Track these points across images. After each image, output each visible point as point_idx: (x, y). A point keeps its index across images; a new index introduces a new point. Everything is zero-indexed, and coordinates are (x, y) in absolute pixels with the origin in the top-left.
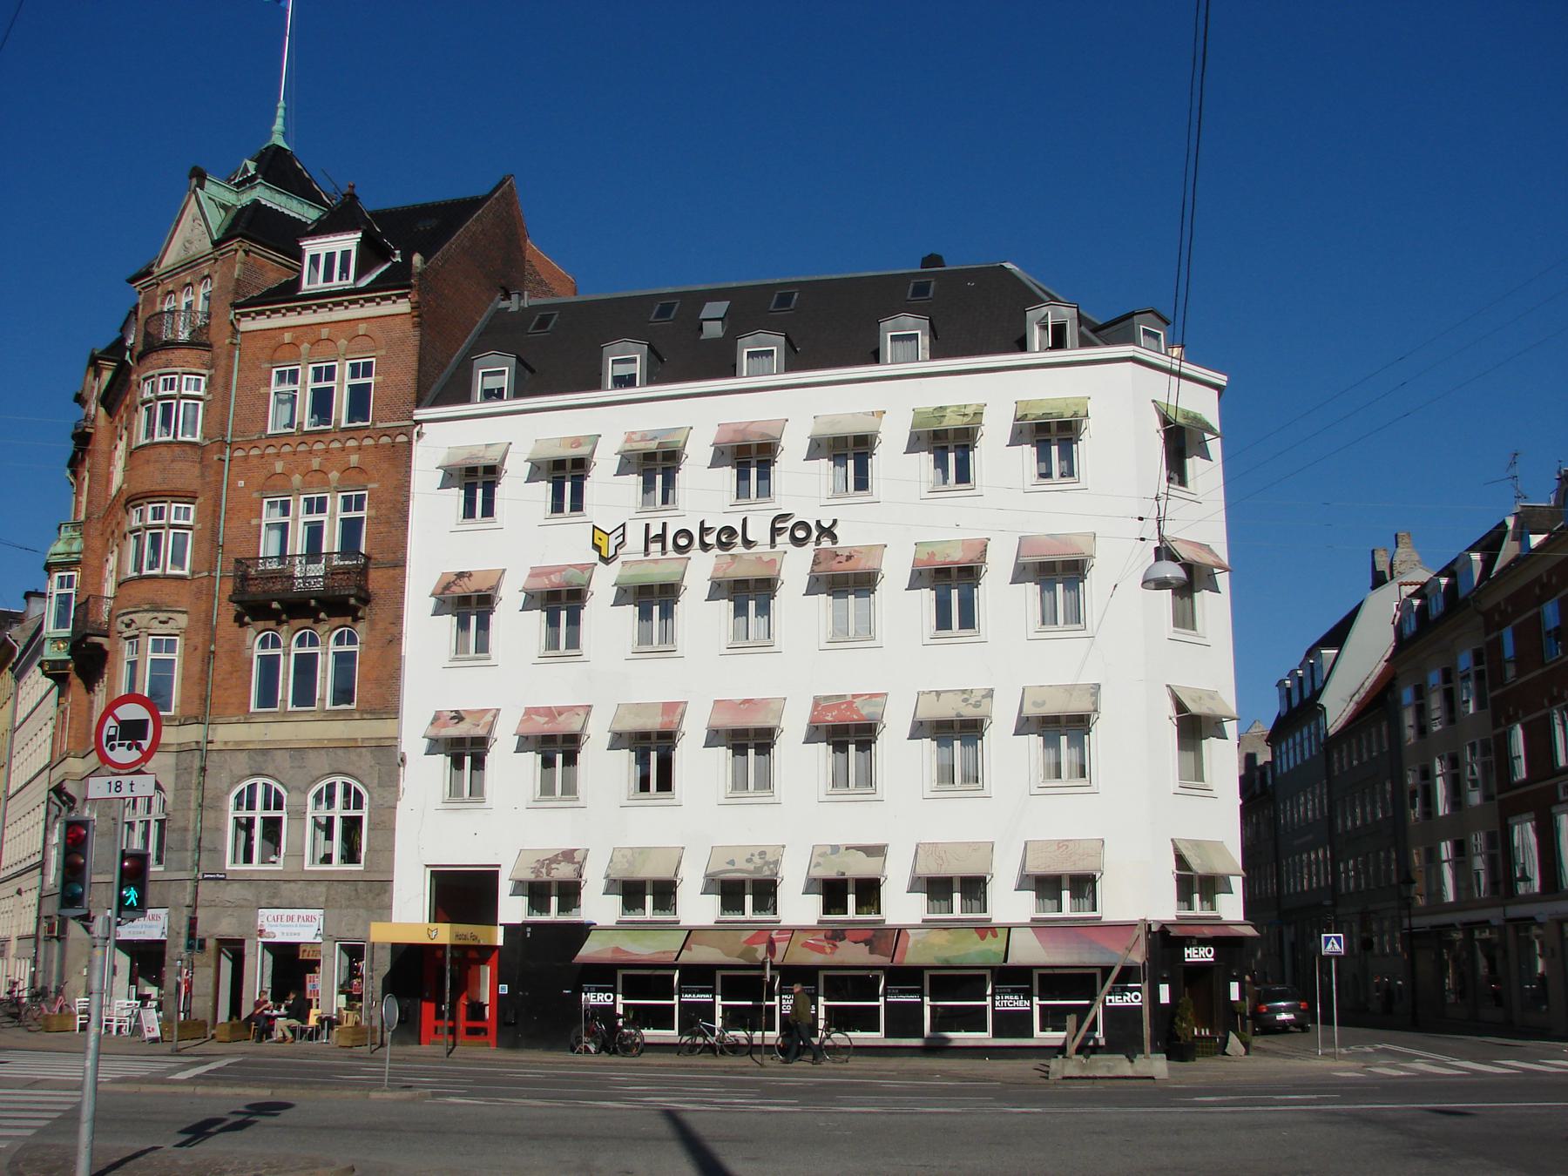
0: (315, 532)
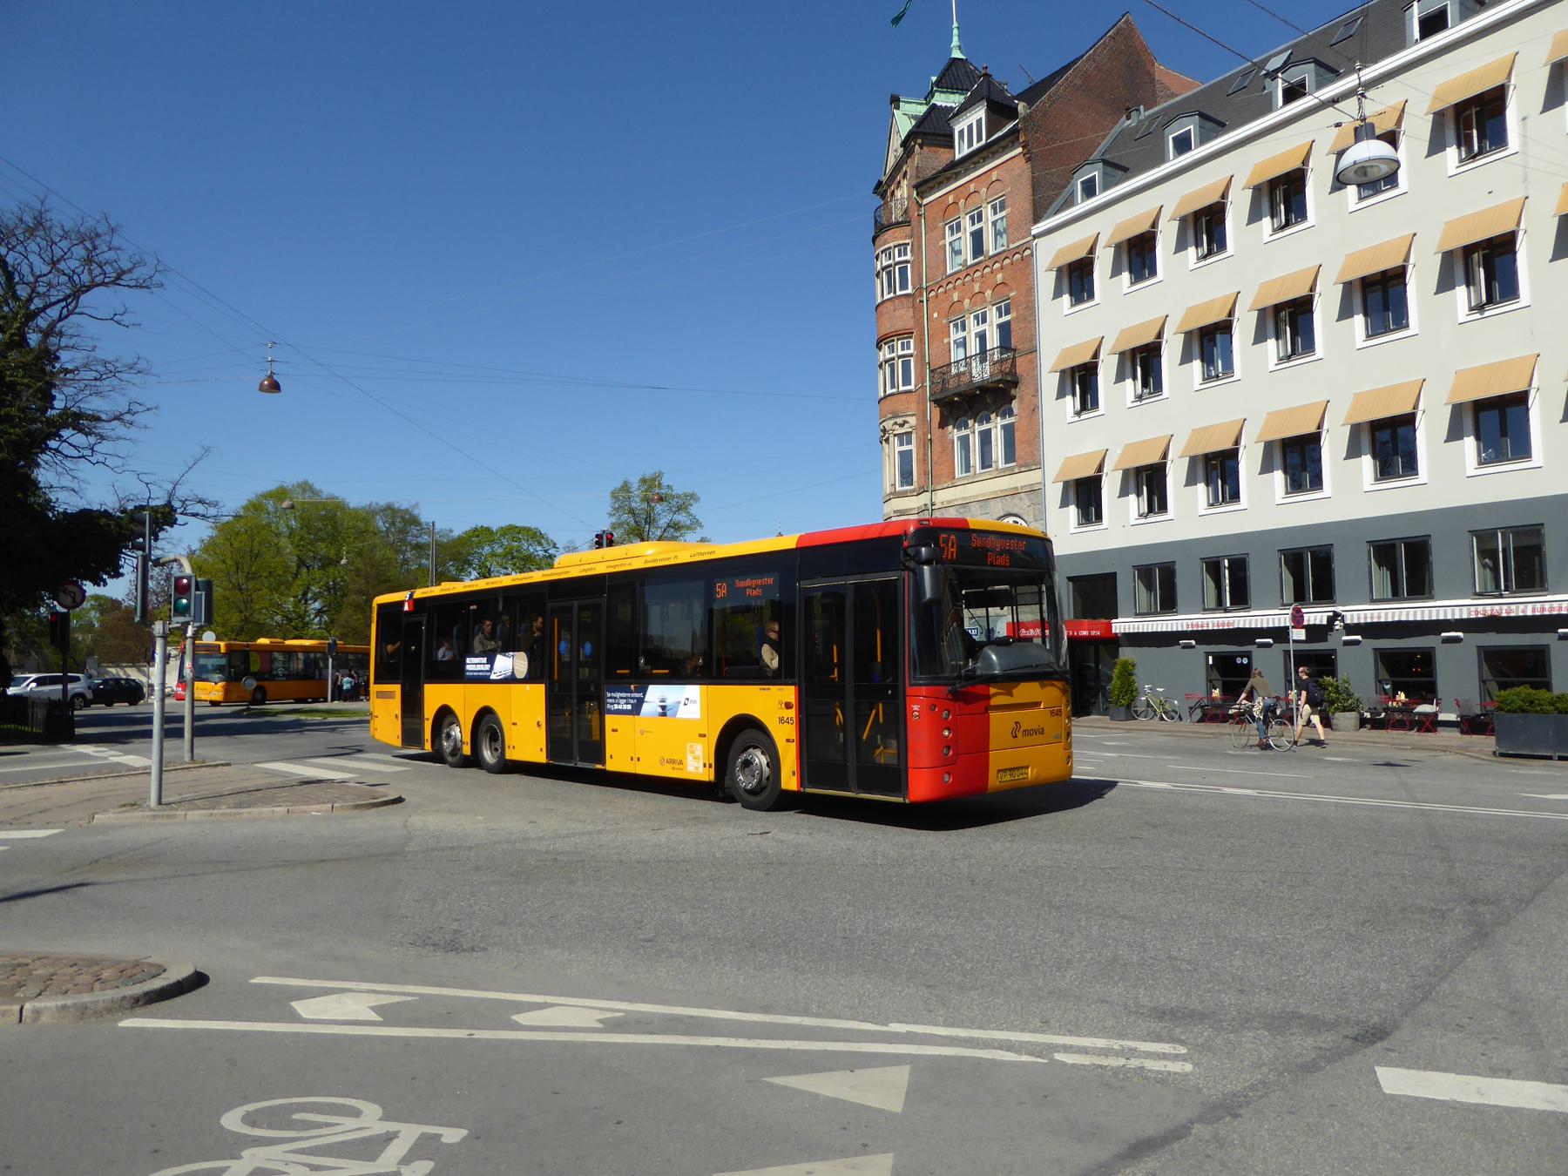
0: (982, 337)
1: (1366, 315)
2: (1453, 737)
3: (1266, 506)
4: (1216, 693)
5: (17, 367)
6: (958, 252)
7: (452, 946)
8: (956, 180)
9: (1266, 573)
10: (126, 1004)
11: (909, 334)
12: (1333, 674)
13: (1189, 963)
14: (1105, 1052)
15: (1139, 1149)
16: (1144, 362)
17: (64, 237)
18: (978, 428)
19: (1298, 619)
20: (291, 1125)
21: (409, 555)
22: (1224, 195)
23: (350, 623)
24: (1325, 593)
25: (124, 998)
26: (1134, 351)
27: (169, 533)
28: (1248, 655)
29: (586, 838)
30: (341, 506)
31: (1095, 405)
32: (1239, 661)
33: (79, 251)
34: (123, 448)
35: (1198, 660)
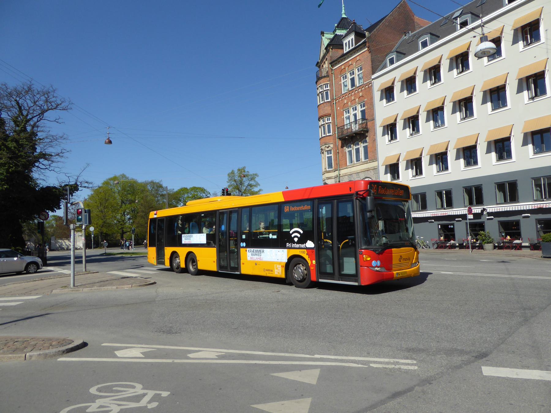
0: (355, 115)
1: (492, 102)
2: (527, 251)
3: (458, 171)
4: (442, 238)
5: (23, 138)
6: (346, 86)
7: (170, 332)
8: (345, 60)
9: (459, 195)
10: (60, 353)
11: (330, 115)
12: (484, 230)
13: (421, 332)
14: (388, 363)
15: (395, 395)
16: (413, 122)
17: (38, 94)
18: (355, 147)
19: (470, 211)
20: (112, 391)
21: (159, 198)
22: (440, 62)
23: (140, 224)
24: (480, 202)
25: (59, 351)
26: (409, 118)
27: (76, 194)
28: (453, 224)
29: (217, 295)
30: (136, 182)
31: (396, 138)
32: (450, 227)
33: (43, 98)
34: (60, 164)
35: (435, 226)
